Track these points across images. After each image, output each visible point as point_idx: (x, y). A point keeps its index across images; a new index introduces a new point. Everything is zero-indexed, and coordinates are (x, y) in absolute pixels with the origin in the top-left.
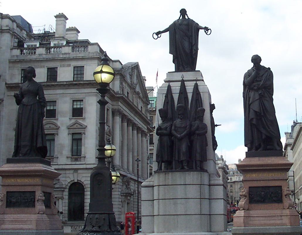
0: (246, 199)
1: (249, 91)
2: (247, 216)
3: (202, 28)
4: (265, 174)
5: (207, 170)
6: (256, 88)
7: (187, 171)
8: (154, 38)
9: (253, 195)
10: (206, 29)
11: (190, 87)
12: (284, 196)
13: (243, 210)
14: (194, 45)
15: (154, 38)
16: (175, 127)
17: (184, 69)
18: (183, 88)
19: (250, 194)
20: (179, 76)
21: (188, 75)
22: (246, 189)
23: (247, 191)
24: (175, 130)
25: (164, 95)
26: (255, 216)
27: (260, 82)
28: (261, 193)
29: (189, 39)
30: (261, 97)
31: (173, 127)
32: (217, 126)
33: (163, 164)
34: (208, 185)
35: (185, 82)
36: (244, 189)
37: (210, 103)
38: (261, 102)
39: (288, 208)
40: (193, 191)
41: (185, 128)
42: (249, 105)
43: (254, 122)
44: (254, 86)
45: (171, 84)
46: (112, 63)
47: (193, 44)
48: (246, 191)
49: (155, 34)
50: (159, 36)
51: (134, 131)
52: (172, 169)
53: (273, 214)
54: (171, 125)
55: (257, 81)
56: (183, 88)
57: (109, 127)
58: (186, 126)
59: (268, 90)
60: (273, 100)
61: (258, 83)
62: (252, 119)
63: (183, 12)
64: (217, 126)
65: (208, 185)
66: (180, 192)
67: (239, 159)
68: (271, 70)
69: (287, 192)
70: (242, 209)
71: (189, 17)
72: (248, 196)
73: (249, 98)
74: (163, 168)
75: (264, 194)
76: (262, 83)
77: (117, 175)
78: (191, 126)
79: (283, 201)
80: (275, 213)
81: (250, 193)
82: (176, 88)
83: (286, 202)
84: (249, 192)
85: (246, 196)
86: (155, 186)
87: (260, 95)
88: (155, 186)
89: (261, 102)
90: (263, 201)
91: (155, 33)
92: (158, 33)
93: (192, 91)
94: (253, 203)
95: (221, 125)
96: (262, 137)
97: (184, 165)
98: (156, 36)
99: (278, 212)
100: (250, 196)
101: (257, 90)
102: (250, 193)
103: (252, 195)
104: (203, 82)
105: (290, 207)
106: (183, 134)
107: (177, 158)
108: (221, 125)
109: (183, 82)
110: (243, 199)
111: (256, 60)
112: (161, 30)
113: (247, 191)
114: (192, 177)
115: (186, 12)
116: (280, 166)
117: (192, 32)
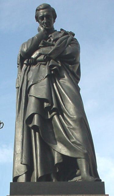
1: (29, 71)
43: (35, 122)
55: (45, 45)
62: (32, 116)
73: (28, 82)
87: (50, 68)
111: (47, 16)
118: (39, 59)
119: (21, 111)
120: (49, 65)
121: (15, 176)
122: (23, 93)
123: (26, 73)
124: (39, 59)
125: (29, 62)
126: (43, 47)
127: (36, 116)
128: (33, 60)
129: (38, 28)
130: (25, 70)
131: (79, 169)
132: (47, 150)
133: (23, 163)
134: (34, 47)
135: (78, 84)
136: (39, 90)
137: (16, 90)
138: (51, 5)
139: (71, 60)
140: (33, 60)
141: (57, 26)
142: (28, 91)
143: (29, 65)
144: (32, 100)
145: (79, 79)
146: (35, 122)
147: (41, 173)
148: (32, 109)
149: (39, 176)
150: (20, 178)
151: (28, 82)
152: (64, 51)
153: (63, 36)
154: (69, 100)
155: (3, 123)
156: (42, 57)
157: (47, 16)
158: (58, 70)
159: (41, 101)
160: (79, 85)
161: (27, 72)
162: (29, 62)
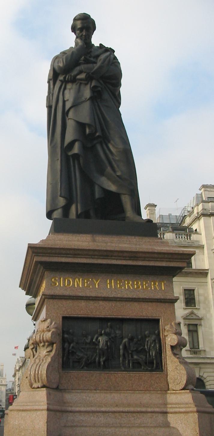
1: (65, 89)
2: (58, 408)
4: (110, 283)
9: (73, 341)
19: (64, 340)
26: (83, 409)
27: (95, 65)
30: (96, 97)
38: (97, 113)
39: (183, 389)
44: (81, 72)
48: (53, 330)
51: (186, 263)
59: (111, 87)
61: (90, 65)
62: (71, 145)
67: (29, 244)
68: (115, 53)
73: (64, 102)
76: (96, 66)
77: (163, 221)
79: (56, 234)
81: (66, 336)
84: (63, 332)
85: (51, 344)
87: (94, 90)
89: (97, 113)
90: (104, 362)
94: (74, 368)
96: (93, 194)
100: (66, 345)
102: (66, 336)
103: (70, 344)
111: (84, 26)
113: (56, 328)
116: (144, 259)
118: (78, 77)
120: (92, 86)
122: (193, 264)
123: (61, 93)
124: (78, 77)
125: (66, 79)
126: (84, 64)
128: (71, 77)
129: (170, 346)
135: (120, 109)
138: (94, 44)
139: (114, 81)
140: (72, 78)
141: (96, 40)
142: (65, 114)
143: (65, 82)
144: (71, 125)
146: (76, 149)
151: (64, 102)
156: (83, 76)
157: (84, 26)
159: (81, 126)
161: (62, 89)
162: (66, 79)
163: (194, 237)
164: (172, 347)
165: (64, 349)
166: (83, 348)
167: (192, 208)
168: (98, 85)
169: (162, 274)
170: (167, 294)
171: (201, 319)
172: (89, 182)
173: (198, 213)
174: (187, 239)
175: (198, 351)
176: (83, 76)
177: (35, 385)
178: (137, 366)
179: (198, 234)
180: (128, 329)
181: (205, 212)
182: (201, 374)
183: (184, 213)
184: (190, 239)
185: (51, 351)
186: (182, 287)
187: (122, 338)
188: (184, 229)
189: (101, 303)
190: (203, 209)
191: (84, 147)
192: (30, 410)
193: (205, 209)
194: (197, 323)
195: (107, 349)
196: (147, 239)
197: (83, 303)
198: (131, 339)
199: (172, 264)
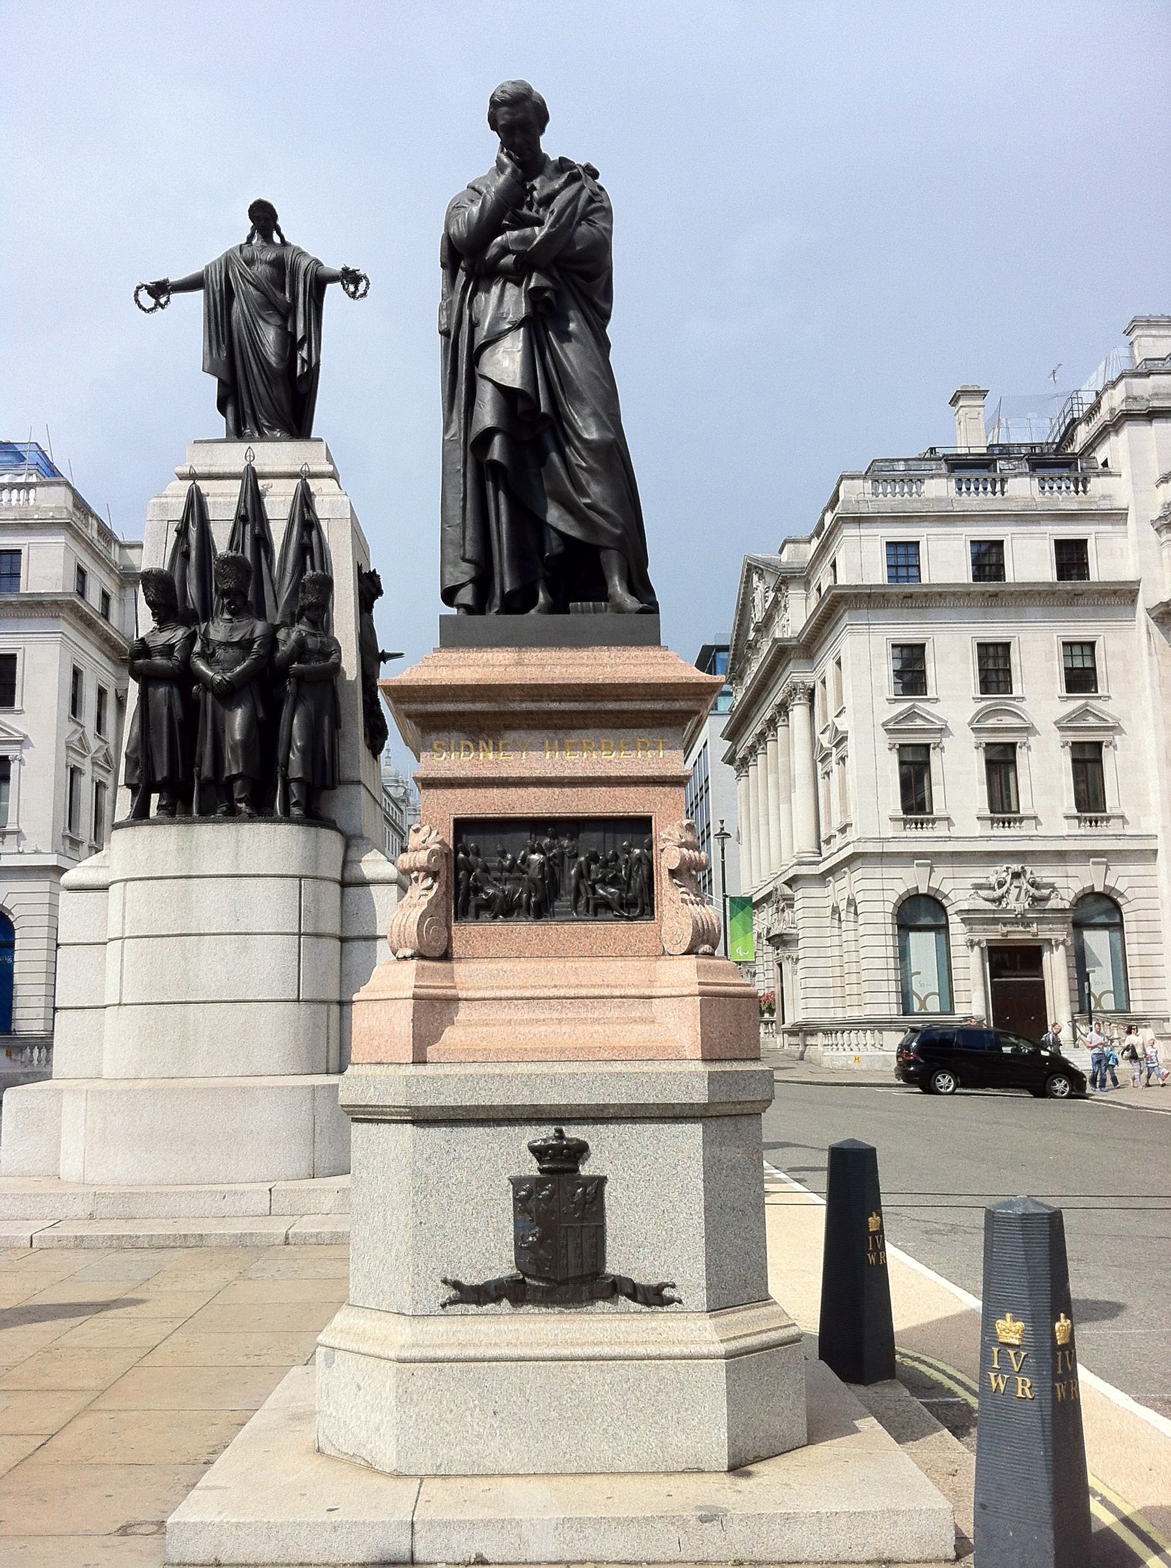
0: (431, 894)
3: (333, 279)
5: (334, 822)
6: (509, 259)
7: (251, 819)
8: (140, 307)
10: (350, 277)
11: (278, 504)
12: (665, 875)
13: (412, 957)
14: (303, 338)
15: (140, 307)
16: (207, 642)
17: (261, 433)
18: (252, 512)
20: (234, 457)
21: (275, 455)
22: (434, 833)
23: (441, 842)
24: (202, 655)
25: (173, 526)
28: (524, 859)
29: (285, 320)
31: (197, 648)
32: (385, 657)
33: (155, 798)
34: (334, 881)
35: (261, 483)
36: (427, 828)
37: (360, 568)
40: (272, 906)
41: (245, 645)
42: (475, 358)
43: (496, 451)
45: (205, 486)
46: (117, 548)
47: (299, 337)
49: (143, 294)
50: (163, 300)
52: (188, 812)
53: (593, 986)
54: (191, 639)
55: (522, 222)
56: (252, 512)
57: (106, 742)
58: (253, 641)
59: (578, 280)
60: (609, 346)
62: (489, 433)
63: (263, 217)
64: (385, 657)
65: (334, 881)
66: (212, 905)
69: (685, 850)
70: (409, 952)
71: (287, 239)
72: (443, 876)
73: (473, 326)
74: (153, 812)
75: (542, 865)
76: (539, 233)
78: (271, 641)
80: (610, 979)
82: (223, 502)
83: (676, 911)
85: (435, 875)
86: (112, 883)
87: (533, 296)
88: (112, 883)
91: (147, 287)
92: (160, 290)
93: (285, 512)
95: (400, 655)
97: (236, 796)
98: (148, 301)
99: (623, 974)
101: (516, 276)
104: (334, 481)
105: (704, 942)
106: (238, 669)
107: (207, 770)
108: (400, 655)
109: (251, 479)
110: (418, 893)
111: (519, 119)
112: (174, 279)
114: (270, 845)
115: (275, 217)
116: (618, 699)
117: (294, 296)
119: (455, 416)
121: (449, 584)
127: (497, 440)
130: (465, 288)
131: (313, 812)
132: (528, 521)
133: (467, 556)
134: (490, 225)
136: (507, 363)
137: (437, 341)
141: (552, 144)
145: (606, 316)
146: (496, 451)
147: (511, 584)
148: (487, 415)
149: (508, 590)
150: (462, 591)
152: (571, 243)
153: (567, 184)
154: (494, 592)
155: (365, 277)
157: (519, 119)
158: (554, 300)
160: (612, 330)
163: (1096, 485)
164: (673, 873)
165: (457, 883)
166: (496, 879)
167: (1097, 394)
168: (545, 282)
169: (661, 725)
170: (668, 765)
171: (1115, 729)
172: (528, 521)
173: (1112, 410)
174: (1077, 492)
175: (1102, 818)
176: (509, 259)
177: (400, 954)
178: (600, 909)
179: (1110, 474)
180: (591, 840)
181: (1135, 407)
182: (1110, 882)
183: (1072, 410)
184: (1085, 492)
185: (430, 888)
186: (1055, 635)
187: (577, 856)
188: (1068, 463)
189: (532, 790)
190: (1128, 398)
191: (512, 444)
192: (606, 997)
193: (1135, 398)
194: (1099, 739)
195: (543, 880)
196: (634, 652)
197: (495, 793)
198: (593, 858)
199: (677, 705)
